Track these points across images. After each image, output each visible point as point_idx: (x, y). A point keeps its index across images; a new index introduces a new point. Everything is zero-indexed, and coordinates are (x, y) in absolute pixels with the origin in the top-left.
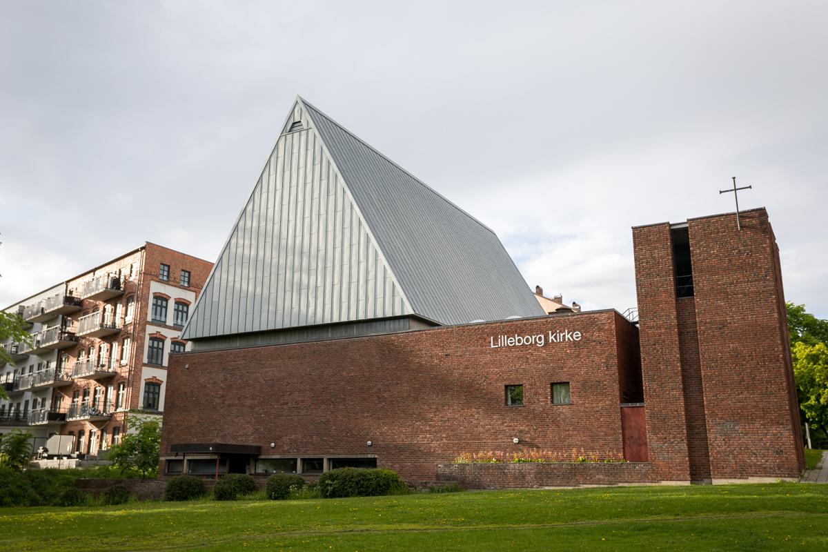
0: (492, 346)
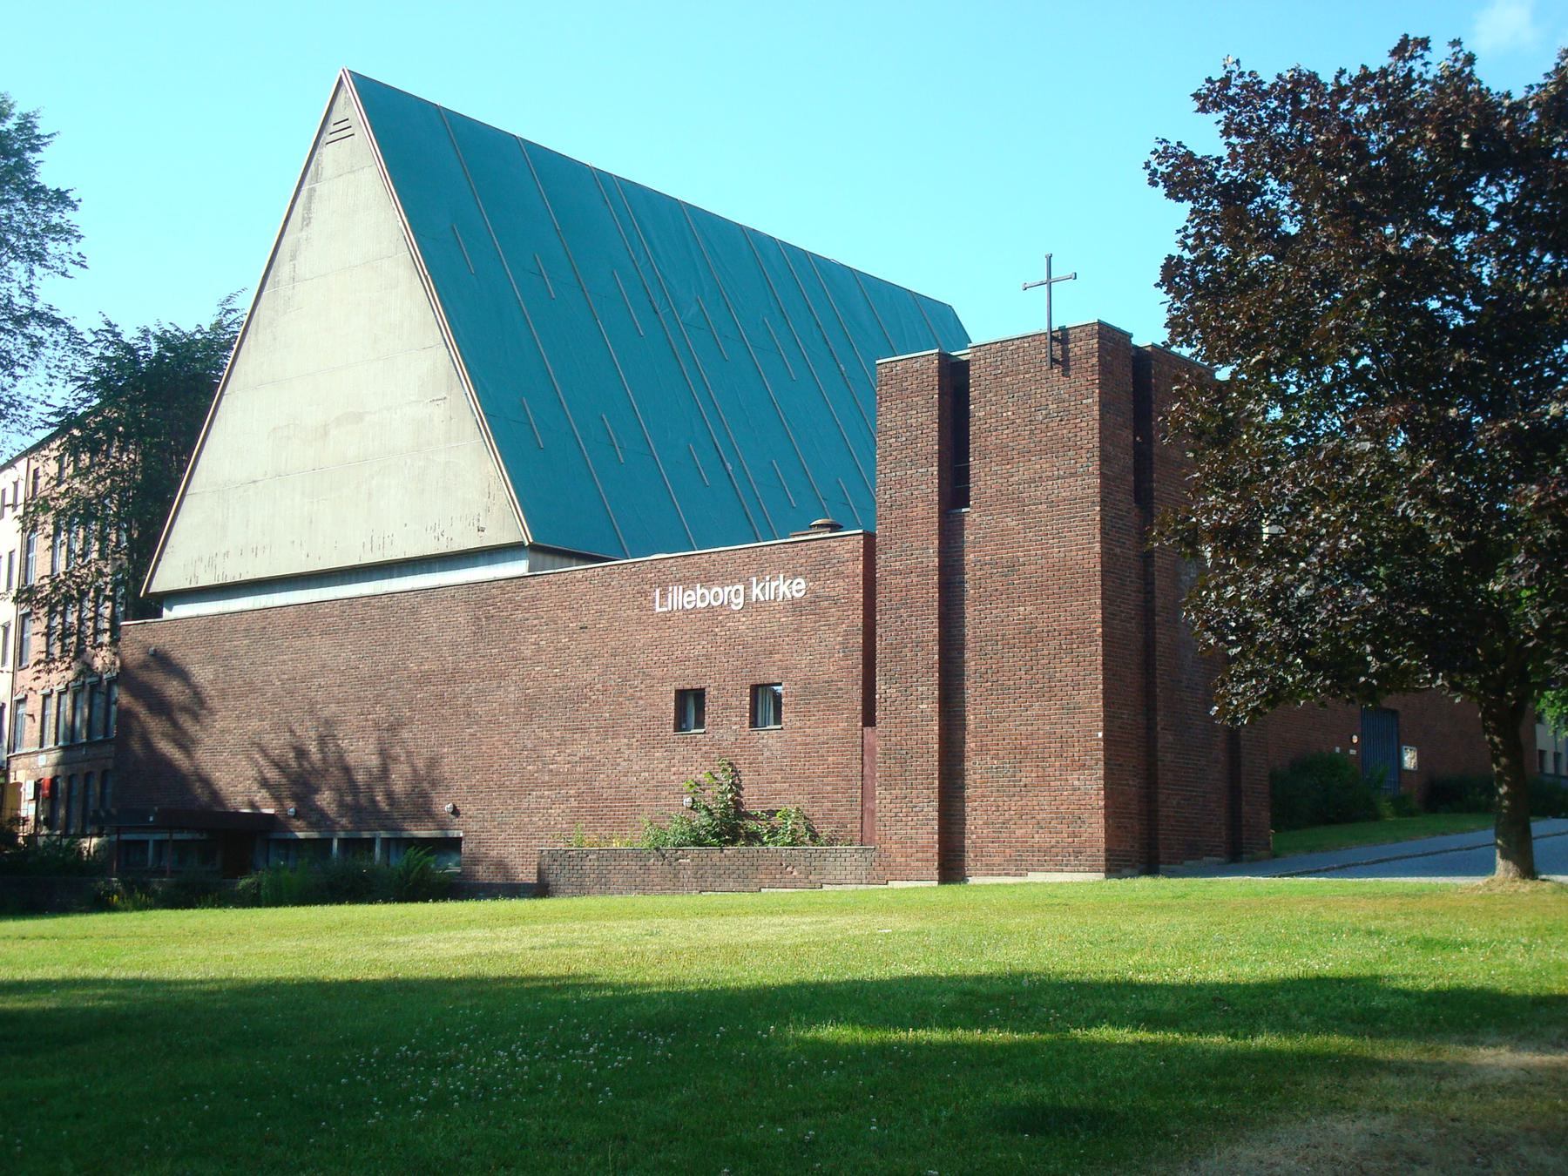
0: (658, 610)
